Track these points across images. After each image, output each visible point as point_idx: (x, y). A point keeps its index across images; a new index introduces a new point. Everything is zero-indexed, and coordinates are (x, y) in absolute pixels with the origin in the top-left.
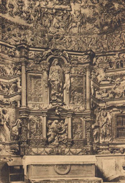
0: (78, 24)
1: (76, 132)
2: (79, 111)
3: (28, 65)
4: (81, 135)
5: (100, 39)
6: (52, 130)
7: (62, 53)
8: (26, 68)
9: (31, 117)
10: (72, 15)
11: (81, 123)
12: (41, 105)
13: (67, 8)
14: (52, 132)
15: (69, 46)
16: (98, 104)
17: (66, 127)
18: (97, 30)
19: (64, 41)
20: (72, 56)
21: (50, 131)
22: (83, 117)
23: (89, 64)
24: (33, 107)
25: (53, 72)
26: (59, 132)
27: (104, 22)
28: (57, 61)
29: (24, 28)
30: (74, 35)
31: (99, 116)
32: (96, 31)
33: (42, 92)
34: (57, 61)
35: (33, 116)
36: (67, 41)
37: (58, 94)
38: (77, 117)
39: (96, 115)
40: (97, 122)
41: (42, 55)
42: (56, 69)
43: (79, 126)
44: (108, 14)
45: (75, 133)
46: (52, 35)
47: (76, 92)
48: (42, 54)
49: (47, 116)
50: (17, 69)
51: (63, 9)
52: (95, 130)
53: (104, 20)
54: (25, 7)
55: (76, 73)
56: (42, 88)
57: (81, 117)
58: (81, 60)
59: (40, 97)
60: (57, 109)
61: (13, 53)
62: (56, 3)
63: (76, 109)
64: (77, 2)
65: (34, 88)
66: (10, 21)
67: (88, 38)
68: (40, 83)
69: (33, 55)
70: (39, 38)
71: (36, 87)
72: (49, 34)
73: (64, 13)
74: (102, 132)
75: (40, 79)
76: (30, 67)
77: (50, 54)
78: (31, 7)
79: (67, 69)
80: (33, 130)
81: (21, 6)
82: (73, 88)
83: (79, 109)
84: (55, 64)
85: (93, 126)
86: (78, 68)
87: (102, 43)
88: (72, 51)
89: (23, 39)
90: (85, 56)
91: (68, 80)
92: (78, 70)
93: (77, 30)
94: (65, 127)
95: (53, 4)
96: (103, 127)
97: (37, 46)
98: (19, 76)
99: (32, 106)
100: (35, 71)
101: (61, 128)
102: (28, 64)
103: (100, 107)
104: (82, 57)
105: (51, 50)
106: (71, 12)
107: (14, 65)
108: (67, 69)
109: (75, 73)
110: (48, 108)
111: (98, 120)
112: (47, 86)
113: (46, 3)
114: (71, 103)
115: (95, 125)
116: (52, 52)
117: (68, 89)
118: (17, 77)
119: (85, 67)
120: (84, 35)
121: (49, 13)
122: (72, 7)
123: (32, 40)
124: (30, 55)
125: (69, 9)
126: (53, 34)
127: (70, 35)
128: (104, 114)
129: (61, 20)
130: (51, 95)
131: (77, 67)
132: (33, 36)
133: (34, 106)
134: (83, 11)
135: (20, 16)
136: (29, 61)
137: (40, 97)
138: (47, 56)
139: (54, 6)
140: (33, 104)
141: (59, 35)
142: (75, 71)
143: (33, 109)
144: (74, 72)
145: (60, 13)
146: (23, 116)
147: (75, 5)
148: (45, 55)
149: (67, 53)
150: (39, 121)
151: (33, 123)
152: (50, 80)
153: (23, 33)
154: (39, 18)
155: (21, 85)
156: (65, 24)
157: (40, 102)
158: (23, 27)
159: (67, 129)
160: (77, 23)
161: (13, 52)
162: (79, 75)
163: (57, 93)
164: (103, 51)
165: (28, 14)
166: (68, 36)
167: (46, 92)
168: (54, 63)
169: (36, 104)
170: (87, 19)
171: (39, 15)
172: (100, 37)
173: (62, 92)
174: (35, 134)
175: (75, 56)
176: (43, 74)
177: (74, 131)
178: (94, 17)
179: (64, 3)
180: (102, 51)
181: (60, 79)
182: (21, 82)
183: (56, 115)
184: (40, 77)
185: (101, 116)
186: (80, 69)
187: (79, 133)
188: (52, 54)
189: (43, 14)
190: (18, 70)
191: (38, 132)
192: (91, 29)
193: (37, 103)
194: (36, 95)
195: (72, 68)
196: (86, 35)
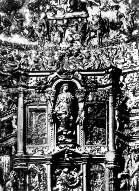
0: (98, 33)
1: (95, 184)
2: (100, 154)
3: (27, 96)
4: (102, 188)
5: (129, 49)
6: (61, 182)
7: (74, 75)
8: (25, 100)
9: (31, 166)
10: (89, 22)
11: (102, 172)
12: (44, 148)
13: (82, 14)
14: (60, 185)
15: (87, 64)
16: (126, 143)
17: (81, 177)
18: (124, 36)
19: (80, 58)
20: (89, 77)
21: (58, 184)
22: (104, 163)
23: (111, 86)
24: (34, 152)
25: (60, 102)
26: (71, 184)
27: (132, 24)
28: (66, 86)
29: (25, 48)
30: (94, 47)
31: (128, 160)
32: (123, 39)
33: (47, 131)
34: (66, 86)
35: (33, 164)
36: (84, 57)
37: (67, 132)
38: (96, 163)
39: (125, 159)
40: (125, 169)
41: (46, 80)
42: (64, 98)
43: (99, 175)
44: (136, 12)
45: (93, 185)
46: (64, 52)
47: (95, 127)
48: (46, 79)
49: (51, 163)
50: (13, 103)
51: (76, 17)
52: (122, 181)
53: (131, 22)
54: (26, 22)
55: (95, 99)
56: (46, 126)
57: (103, 162)
58: (102, 81)
59: (43, 138)
60: (66, 154)
61: (8, 82)
62: (67, 10)
63: (94, 151)
64: (95, 5)
65: (35, 126)
66: (6, 42)
67: (112, 49)
68: (44, 118)
69: (35, 81)
70: (45, 58)
71: (39, 125)
72: (59, 51)
73: (78, 21)
74: (132, 184)
75: (44, 113)
76: (31, 98)
77: (56, 78)
78: (34, 20)
79: (81, 96)
80: (34, 184)
81: (20, 22)
82: (90, 121)
83: (99, 151)
84: (64, 91)
85: (119, 176)
86: (98, 92)
87: (131, 53)
88: (89, 70)
89: (23, 62)
90: (106, 75)
91: (82, 111)
92: (98, 96)
93: (97, 41)
94: (80, 178)
95: (63, 12)
96: (134, 176)
97: (42, 69)
98: (15, 112)
99: (33, 151)
100: (37, 103)
101: (73, 179)
102: (27, 95)
103: (129, 147)
104: (103, 77)
105: (58, 73)
106: (88, 19)
107: (10, 98)
108: (81, 96)
109: (93, 100)
110: (53, 153)
111: (128, 167)
112: (52, 121)
113: (54, 13)
114: (88, 142)
115: (122, 174)
116: (59, 76)
117: (83, 123)
118: (12, 113)
119: (107, 90)
120: (107, 46)
121: (59, 25)
122: (89, 12)
123: (35, 62)
124: (30, 82)
125: (85, 16)
126: (65, 50)
127: (89, 49)
128: (135, 157)
129: (75, 32)
130: (59, 134)
131: (96, 91)
132: (38, 56)
133: (35, 151)
134: (104, 15)
135: (20, 33)
136: (29, 90)
137: (43, 138)
138: (53, 81)
139: (64, 16)
140: (34, 148)
141: (74, 51)
142: (93, 97)
143: (34, 155)
144: (92, 98)
145: (74, 22)
146: (18, 167)
147: (92, 8)
148: (50, 81)
149: (81, 74)
150: (42, 171)
151: (34, 173)
152: (56, 113)
153: (24, 54)
154: (45, 33)
155: (16, 124)
156: (81, 36)
157: (44, 144)
158: (23, 47)
159: (81, 181)
160: (95, 32)
161: (8, 81)
162: (98, 103)
163: (65, 132)
164: (131, 65)
165: (30, 30)
166: (86, 51)
167: (52, 129)
168: (62, 90)
169: (38, 147)
170: (110, 25)
171: (46, 30)
172: (128, 46)
173: (74, 128)
174: (37, 188)
175: (93, 77)
176: (48, 106)
177: (92, 182)
178: (119, 21)
179: (78, 8)
180: (129, 66)
181: (70, 110)
182: (17, 119)
183: (67, 162)
184: (44, 111)
185: (131, 161)
186: (101, 94)
187: (99, 184)
188: (59, 78)
189: (51, 27)
190: (13, 104)
191: (41, 186)
192: (116, 37)
193: (40, 147)
194: (39, 136)
195: (89, 94)
196: (109, 46)
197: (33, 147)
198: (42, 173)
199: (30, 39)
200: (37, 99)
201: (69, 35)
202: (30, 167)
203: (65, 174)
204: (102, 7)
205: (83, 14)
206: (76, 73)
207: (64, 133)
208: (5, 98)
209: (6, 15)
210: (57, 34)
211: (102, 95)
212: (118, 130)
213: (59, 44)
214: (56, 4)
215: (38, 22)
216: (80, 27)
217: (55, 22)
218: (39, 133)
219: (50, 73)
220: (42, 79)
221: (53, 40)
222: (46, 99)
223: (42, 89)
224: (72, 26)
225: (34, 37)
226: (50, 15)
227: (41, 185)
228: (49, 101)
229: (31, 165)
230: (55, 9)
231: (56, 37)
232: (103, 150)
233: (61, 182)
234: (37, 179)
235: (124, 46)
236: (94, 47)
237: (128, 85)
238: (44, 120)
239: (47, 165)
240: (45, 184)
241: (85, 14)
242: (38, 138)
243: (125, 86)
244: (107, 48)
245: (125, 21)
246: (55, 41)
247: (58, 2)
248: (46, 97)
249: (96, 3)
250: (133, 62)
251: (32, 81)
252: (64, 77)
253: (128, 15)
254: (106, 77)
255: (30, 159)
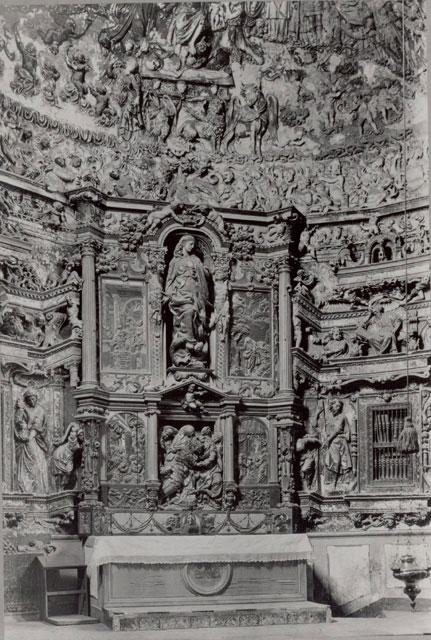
0: (253, 128)
4: (263, 472)
9: (111, 415)
10: (235, 100)
13: (221, 78)
15: (227, 196)
17: (219, 446)
18: (311, 144)
19: (212, 181)
24: (118, 385)
25: (177, 275)
26: (198, 461)
27: (332, 120)
30: (242, 160)
31: (318, 411)
32: (308, 150)
33: (145, 338)
36: (221, 180)
43: (257, 443)
46: (174, 160)
48: (144, 220)
49: (159, 412)
54: (92, 76)
55: (249, 278)
57: (264, 416)
59: (138, 356)
67: (284, 169)
69: (118, 223)
70: (134, 171)
73: (210, 93)
74: (327, 462)
84: (184, 252)
85: (300, 445)
88: (235, 210)
89: (87, 173)
96: (332, 445)
106: (231, 91)
110: (163, 390)
113: (157, 64)
114: (232, 371)
116: (174, 215)
119: (276, 260)
124: (106, 223)
125: (226, 82)
129: (201, 117)
133: (120, 383)
134: (269, 87)
137: (138, 356)
139: (179, 73)
140: (119, 376)
142: (245, 271)
143: (117, 392)
145: (199, 94)
146: (86, 414)
147: (242, 67)
148: (154, 225)
153: (87, 155)
155: (80, 317)
156: (215, 128)
159: (220, 455)
162: (256, 286)
163: (191, 342)
164: (330, 210)
175: (245, 227)
179: (212, 61)
184: (137, 293)
189: (147, 96)
194: (127, 349)
197: (116, 374)
198: (133, 433)
199: (100, 118)
200: (123, 265)
201: (187, 122)
202: (108, 417)
203: (186, 439)
204: (265, 67)
205: (220, 75)
206: (211, 214)
207: (189, 345)
208: (50, 255)
209: (49, 51)
210: (161, 117)
211: (263, 269)
212: (301, 346)
213: (165, 140)
214: (162, 41)
215: (119, 81)
216: (214, 108)
217: (157, 84)
218: (127, 342)
219: (154, 206)
220: (135, 219)
221: (151, 129)
222: (143, 267)
223: (135, 242)
224: (195, 102)
225: (110, 115)
226: (147, 66)
227: (133, 460)
228: (149, 272)
229: (112, 414)
230: (159, 53)
231: (159, 123)
232: (266, 389)
233: (176, 456)
234: (123, 443)
235: (311, 166)
236: (242, 160)
237: (318, 253)
238: (138, 315)
239: (148, 415)
240: (141, 459)
241: (228, 78)
242: (127, 354)
243: (312, 253)
244: (271, 164)
245: (315, 110)
246: (154, 131)
247: (169, 37)
248: (142, 262)
249: (255, 57)
250: (332, 204)
251: (111, 221)
252: (186, 221)
253: (324, 99)
254: (272, 230)
255: (111, 399)
